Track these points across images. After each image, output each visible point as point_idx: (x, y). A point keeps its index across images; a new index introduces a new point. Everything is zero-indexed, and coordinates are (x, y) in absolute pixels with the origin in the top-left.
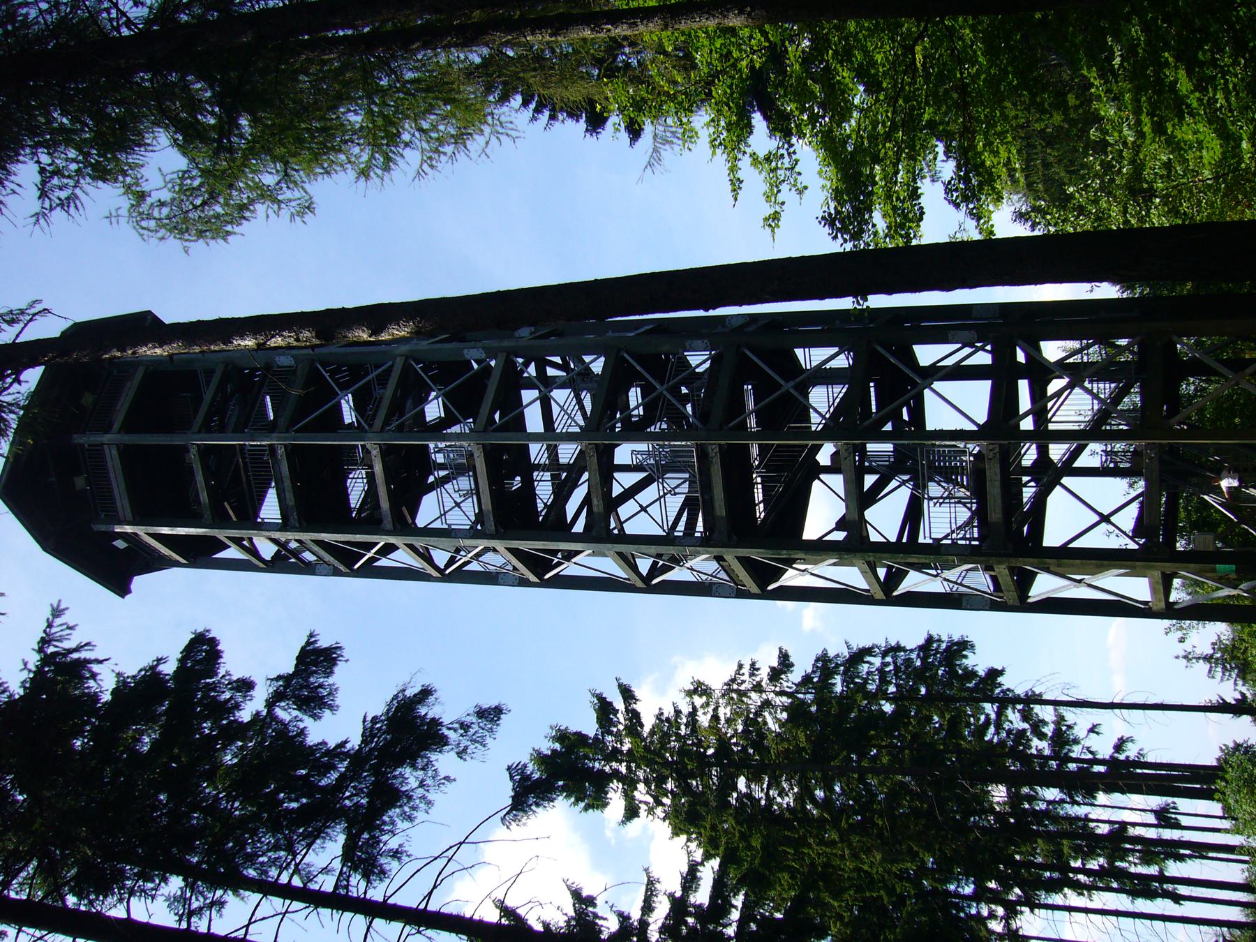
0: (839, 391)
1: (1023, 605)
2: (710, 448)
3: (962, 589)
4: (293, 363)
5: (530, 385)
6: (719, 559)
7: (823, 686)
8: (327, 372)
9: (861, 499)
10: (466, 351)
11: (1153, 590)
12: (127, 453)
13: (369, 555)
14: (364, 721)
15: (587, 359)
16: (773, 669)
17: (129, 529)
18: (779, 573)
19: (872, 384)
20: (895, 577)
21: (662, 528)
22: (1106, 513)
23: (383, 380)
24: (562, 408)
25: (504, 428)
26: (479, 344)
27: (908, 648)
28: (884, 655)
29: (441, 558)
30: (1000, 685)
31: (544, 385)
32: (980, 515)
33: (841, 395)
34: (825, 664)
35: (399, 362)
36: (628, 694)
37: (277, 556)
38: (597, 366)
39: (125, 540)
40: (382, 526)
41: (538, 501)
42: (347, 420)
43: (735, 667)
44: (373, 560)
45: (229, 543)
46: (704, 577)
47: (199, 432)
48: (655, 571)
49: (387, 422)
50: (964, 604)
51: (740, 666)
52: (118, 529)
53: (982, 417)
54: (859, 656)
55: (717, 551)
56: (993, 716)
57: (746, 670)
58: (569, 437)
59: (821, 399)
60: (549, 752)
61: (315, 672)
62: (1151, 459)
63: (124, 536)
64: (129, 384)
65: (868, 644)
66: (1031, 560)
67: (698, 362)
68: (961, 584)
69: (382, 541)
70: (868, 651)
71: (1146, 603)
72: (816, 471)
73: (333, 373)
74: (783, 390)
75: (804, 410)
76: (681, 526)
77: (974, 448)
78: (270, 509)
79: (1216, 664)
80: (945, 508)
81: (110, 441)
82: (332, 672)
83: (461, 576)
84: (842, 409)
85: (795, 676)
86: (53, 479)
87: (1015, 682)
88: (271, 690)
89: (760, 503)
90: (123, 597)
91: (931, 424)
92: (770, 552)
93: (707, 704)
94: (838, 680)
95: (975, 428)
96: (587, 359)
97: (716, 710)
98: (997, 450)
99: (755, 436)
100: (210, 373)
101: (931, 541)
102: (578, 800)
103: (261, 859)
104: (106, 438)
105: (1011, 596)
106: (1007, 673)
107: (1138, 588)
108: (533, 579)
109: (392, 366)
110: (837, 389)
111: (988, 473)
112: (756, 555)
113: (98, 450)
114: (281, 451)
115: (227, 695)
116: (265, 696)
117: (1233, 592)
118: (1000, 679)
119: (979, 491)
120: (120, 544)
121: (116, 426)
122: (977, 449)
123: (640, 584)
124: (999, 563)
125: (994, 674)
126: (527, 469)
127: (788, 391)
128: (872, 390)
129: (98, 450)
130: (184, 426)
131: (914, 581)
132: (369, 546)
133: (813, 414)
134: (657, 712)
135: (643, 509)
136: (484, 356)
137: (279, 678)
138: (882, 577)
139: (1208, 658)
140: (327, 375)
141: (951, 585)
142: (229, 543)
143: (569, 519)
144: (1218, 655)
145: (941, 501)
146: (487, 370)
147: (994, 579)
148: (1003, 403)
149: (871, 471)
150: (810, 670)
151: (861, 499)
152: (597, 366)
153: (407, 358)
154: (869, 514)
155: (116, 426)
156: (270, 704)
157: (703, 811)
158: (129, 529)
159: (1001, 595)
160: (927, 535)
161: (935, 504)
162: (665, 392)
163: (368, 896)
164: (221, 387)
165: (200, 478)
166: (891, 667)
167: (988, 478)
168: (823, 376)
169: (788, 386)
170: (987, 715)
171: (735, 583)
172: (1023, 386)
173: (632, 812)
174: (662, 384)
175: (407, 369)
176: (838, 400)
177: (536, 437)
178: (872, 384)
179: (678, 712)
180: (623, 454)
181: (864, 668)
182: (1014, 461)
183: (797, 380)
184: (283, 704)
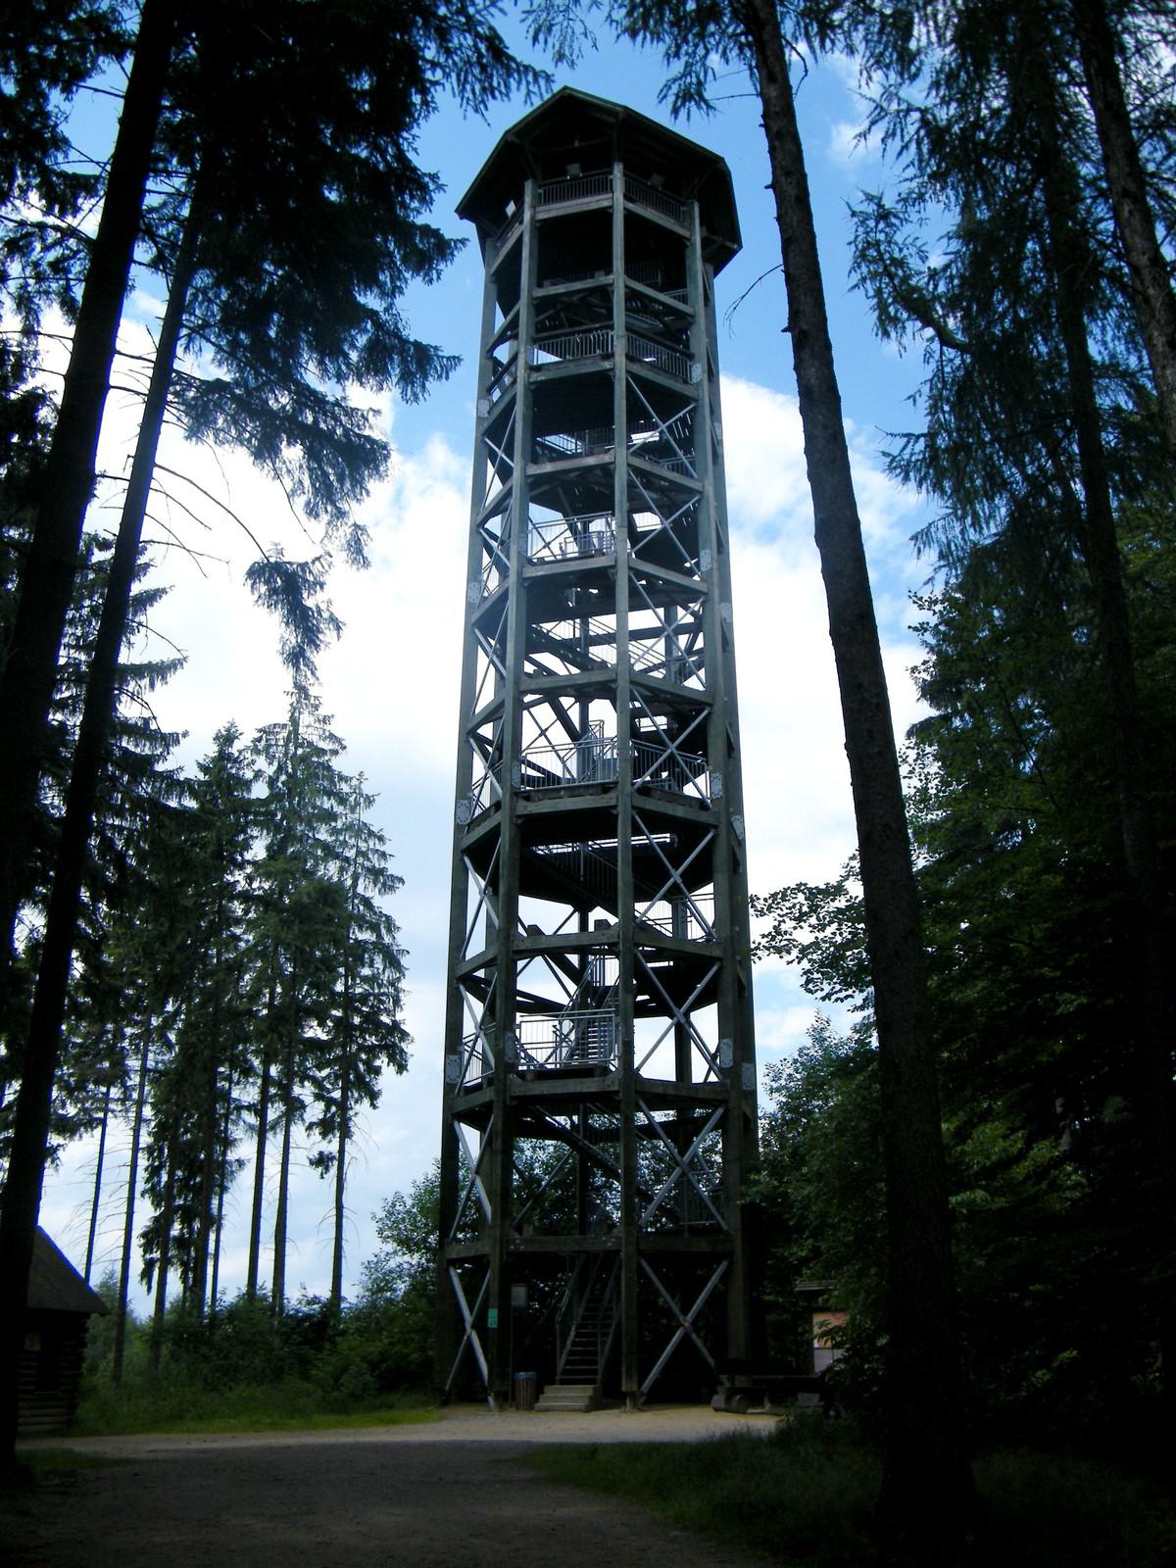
0: (667, 930)
1: (453, 1116)
3: (467, 1055)
4: (694, 381)
5: (670, 617)
6: (497, 806)
8: (685, 415)
9: (555, 952)
10: (708, 551)
12: (604, 216)
13: (500, 453)
15: (702, 673)
18: (481, 871)
19: (672, 963)
20: (478, 988)
21: (528, 748)
23: (679, 468)
24: (650, 649)
25: (633, 592)
26: (715, 566)
29: (495, 525)
31: (667, 631)
32: (542, 1074)
33: (663, 931)
34: (385, 923)
37: (497, 363)
38: (694, 683)
39: (514, 215)
40: (530, 464)
41: (554, 624)
42: (634, 436)
46: (476, 792)
47: (626, 287)
48: (482, 741)
53: (646, 1073)
54: (393, 960)
55: (506, 804)
59: (658, 912)
62: (605, 1242)
64: (673, 221)
66: (500, 1124)
67: (699, 785)
68: (471, 1055)
72: (583, 909)
73: (683, 420)
74: (673, 871)
75: (647, 896)
76: (531, 772)
77: (614, 1065)
78: (545, 358)
80: (551, 1037)
81: (616, 199)
86: (577, 144)
89: (550, 850)
90: (456, 211)
91: (640, 1024)
95: (636, 1065)
96: (702, 673)
100: (684, 299)
101: (518, 1022)
105: (462, 1105)
109: (692, 477)
110: (670, 927)
111: (589, 1080)
112: (504, 842)
113: (606, 187)
114: (607, 365)
117: (468, 1326)
119: (564, 1073)
120: (511, 209)
122: (613, 1069)
123: (470, 726)
125: (373, 1096)
126: (584, 612)
127: (670, 876)
128: (666, 964)
131: (474, 1009)
132: (510, 452)
133: (646, 904)
135: (543, 733)
136: (703, 569)
138: (477, 974)
140: (681, 414)
141: (470, 1044)
142: (509, 317)
143: (83, 1274)
145: (557, 1031)
146: (690, 573)
147: (478, 1087)
148: (656, 1095)
149: (583, 962)
151: (555, 952)
152: (694, 683)
153: (701, 493)
154: (539, 959)
155: (631, 206)
158: (527, 216)
159: (462, 1094)
160: (525, 1019)
161: (554, 1026)
162: (669, 751)
164: (670, 310)
165: (578, 285)
167: (584, 1080)
169: (676, 876)
171: (471, 823)
175: (691, 492)
176: (658, 927)
178: (672, 963)
180: (602, 711)
182: (596, 1106)
183: (682, 886)
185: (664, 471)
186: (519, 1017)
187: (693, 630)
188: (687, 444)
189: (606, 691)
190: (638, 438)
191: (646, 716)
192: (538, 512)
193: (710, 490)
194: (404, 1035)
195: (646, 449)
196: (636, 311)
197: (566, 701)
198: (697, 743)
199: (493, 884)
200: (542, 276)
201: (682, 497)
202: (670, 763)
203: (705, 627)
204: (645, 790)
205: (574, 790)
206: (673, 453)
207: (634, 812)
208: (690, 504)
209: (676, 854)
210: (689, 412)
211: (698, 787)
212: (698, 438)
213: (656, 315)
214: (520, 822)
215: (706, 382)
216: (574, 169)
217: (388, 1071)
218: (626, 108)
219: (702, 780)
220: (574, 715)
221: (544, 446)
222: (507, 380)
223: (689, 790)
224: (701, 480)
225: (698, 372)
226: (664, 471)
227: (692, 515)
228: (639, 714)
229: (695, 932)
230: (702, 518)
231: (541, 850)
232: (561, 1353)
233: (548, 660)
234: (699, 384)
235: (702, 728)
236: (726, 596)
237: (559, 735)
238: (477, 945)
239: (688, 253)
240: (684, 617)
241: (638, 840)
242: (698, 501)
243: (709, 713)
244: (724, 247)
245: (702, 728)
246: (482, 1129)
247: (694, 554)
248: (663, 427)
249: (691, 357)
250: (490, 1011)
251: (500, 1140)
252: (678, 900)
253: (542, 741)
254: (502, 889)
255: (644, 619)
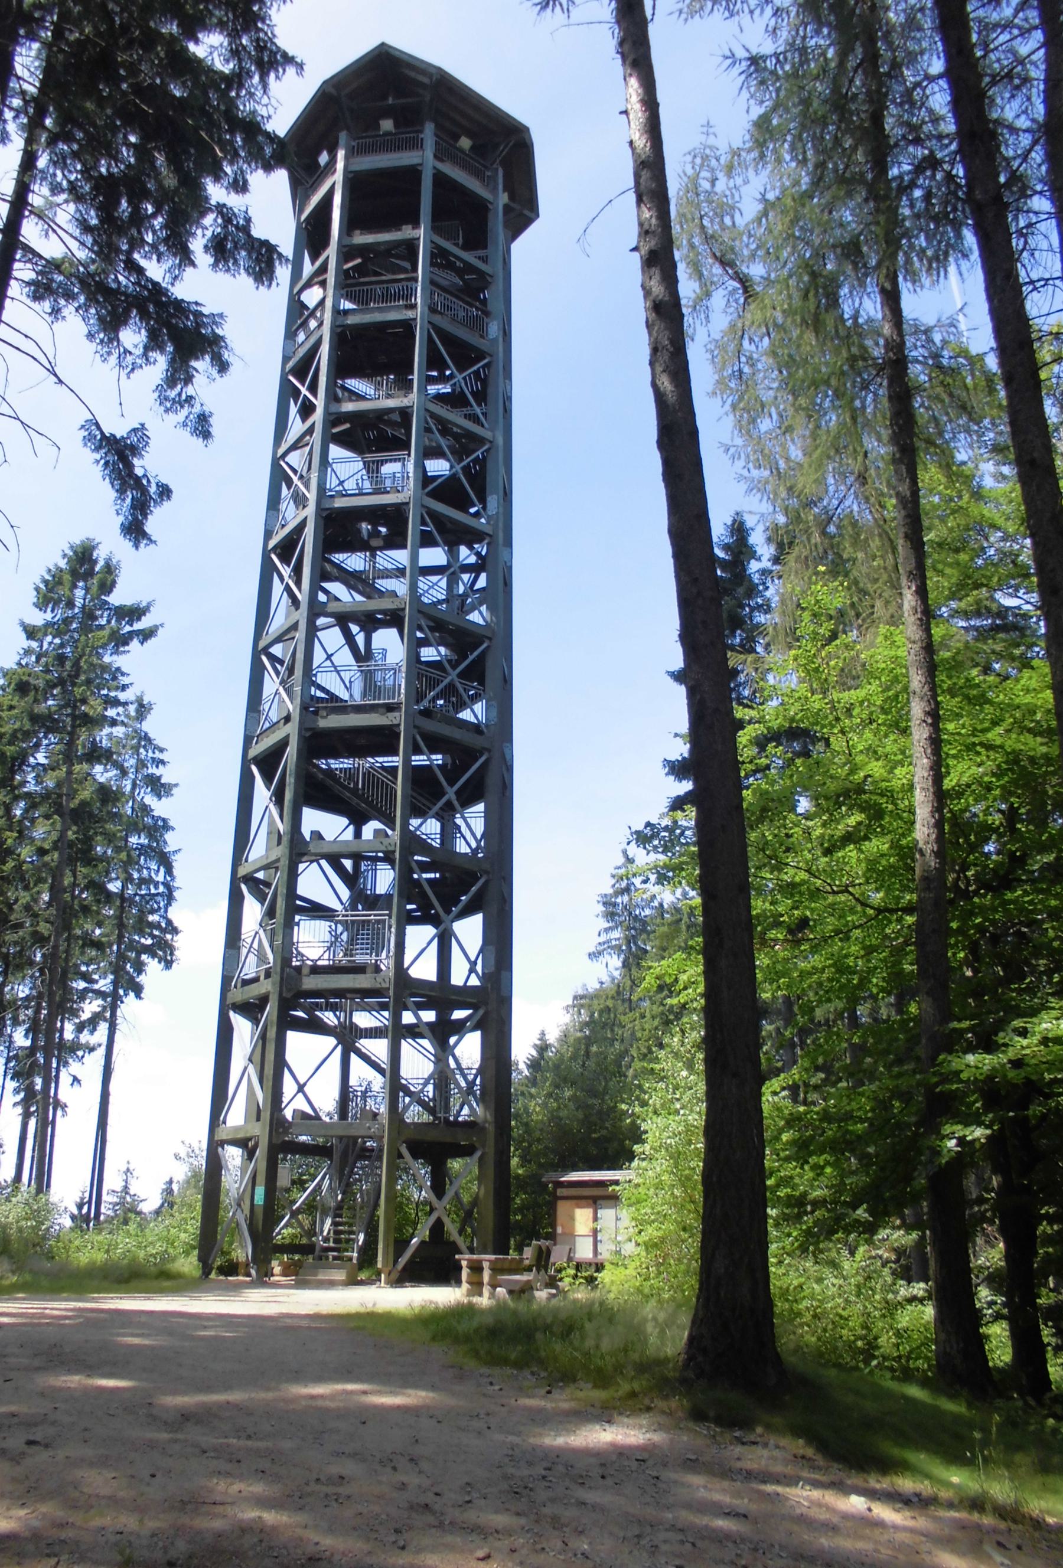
2: (397, 714)
3: (244, 951)
7: (134, 827)
10: (495, 497)
11: (237, 1129)
12: (413, 173)
13: (304, 391)
14: (197, 303)
16: (159, 778)
17: (340, 165)
20: (258, 887)
22: (306, 1089)
23: (474, 418)
26: (501, 510)
27: (170, 909)
28: (166, 885)
29: (296, 459)
30: (126, 995)
31: (450, 571)
34: (159, 828)
35: (488, 435)
36: (147, 635)
37: (304, 306)
39: (327, 164)
41: (345, 555)
43: (162, 745)
44: (297, 392)
45: (318, 263)
46: (267, 708)
48: (273, 658)
49: (433, 415)
50: (231, 952)
51: (161, 750)
52: (341, 154)
54: (165, 861)
56: (96, 987)
57: (158, 755)
58: (413, 587)
60: (95, 555)
61: (250, 257)
63: (333, 160)
65: (175, 872)
69: (319, 403)
70: (169, 871)
71: (224, 1122)
72: (358, 821)
75: (421, 812)
76: (319, 694)
77: (386, 962)
79: (120, 1198)
82: (249, 274)
83: (279, 476)
84: (423, 846)
85: (149, 800)
86: (390, 101)
87: (129, 1005)
88: (236, 211)
91: (411, 930)
92: (293, 767)
93: (128, 716)
94: (144, 840)
95: (406, 965)
97: (123, 723)
98: (384, 985)
99: (407, 761)
100: (484, 260)
102: (46, 582)
103: (59, 173)
104: (429, 153)
105: (237, 995)
106: (138, 1001)
107: (236, 1116)
108: (272, 544)
114: (410, 314)
115: (228, 170)
116: (229, 204)
118: (132, 994)
120: (324, 158)
121: (440, 166)
123: (262, 644)
124: (274, 984)
127: (444, 794)
129: (416, 144)
130: (437, 225)
132: (313, 388)
133: (419, 821)
134: (124, 669)
135: (329, 657)
137: (248, 220)
139: (126, 1189)
140: (475, 368)
142: (318, 263)
144: (128, 1199)
146: (477, 515)
147: (255, 980)
149: (356, 866)
150: (155, 813)
155: (440, 166)
156: (221, 208)
157: (30, 698)
158: (340, 165)
163: (13, 282)
164: (469, 268)
166: (153, 891)
168: (449, 832)
170: (96, 982)
172: (429, 1016)
173: (31, 632)
174: (460, 675)
175: (482, 441)
177: (414, 558)
179: (124, 688)
181: (154, 866)
184: (220, 221)
185: (456, 417)
186: (297, 918)
187: (475, 569)
188: (481, 397)
189: (394, 619)
190: (432, 389)
191: (429, 645)
192: (336, 451)
193: (500, 441)
194: (175, 931)
195: (439, 397)
196: (439, 266)
197: (354, 628)
198: (476, 673)
199: (278, 798)
200: (351, 224)
201: (472, 446)
202: (449, 691)
203: (489, 566)
204: (426, 713)
205: (359, 709)
206: (466, 403)
207: (415, 731)
208: (479, 453)
209: (452, 773)
210: (483, 367)
211: (475, 713)
212: (490, 390)
213: (460, 272)
214: (308, 734)
215: (501, 339)
216: (387, 125)
217: (153, 965)
218: (440, 69)
219: (479, 707)
220: (360, 639)
221: (344, 388)
222: (313, 324)
223: (466, 715)
224: (492, 430)
225: (494, 329)
226: (456, 417)
227: (482, 462)
228: (424, 643)
229: (462, 847)
230: (490, 465)
231: (323, 764)
232: (872, 1494)
233: (337, 588)
234: (496, 340)
235: (481, 659)
236: (509, 543)
237: (345, 657)
238: (258, 850)
239: (490, 216)
240: (465, 555)
241: (419, 760)
242: (487, 451)
243: (488, 647)
244: (521, 215)
245: (481, 659)
246: (256, 1021)
247: (483, 500)
248: (459, 377)
249: (487, 314)
250: (270, 913)
251: (274, 1029)
252: (445, 818)
253: (328, 663)
254: (288, 795)
255: (434, 556)
